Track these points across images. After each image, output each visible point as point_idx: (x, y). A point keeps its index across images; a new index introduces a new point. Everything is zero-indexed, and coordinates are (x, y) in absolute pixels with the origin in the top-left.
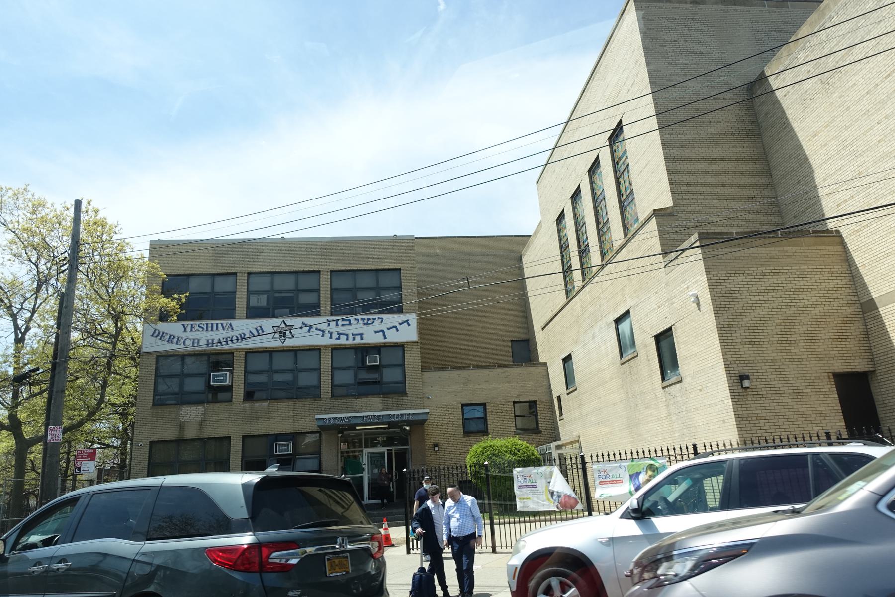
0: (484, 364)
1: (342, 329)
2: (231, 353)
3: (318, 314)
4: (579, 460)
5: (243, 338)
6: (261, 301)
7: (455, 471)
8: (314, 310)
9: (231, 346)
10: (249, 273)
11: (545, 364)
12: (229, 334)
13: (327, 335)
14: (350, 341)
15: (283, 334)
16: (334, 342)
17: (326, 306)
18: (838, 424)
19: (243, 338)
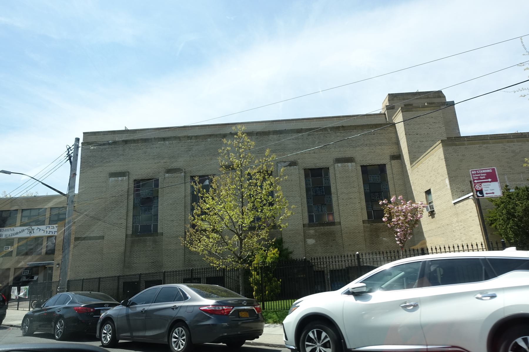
0: (295, 136)
1: (50, 230)
2: (13, 239)
3: (44, 225)
4: (356, 257)
5: (17, 233)
6: (26, 220)
7: (328, 260)
8: (42, 223)
9: (13, 237)
10: (22, 210)
11: (452, 104)
12: (13, 232)
13: (45, 232)
14: (53, 234)
15: (31, 232)
16: (48, 235)
17: (47, 221)
18: (478, 237)
19: (17, 233)
